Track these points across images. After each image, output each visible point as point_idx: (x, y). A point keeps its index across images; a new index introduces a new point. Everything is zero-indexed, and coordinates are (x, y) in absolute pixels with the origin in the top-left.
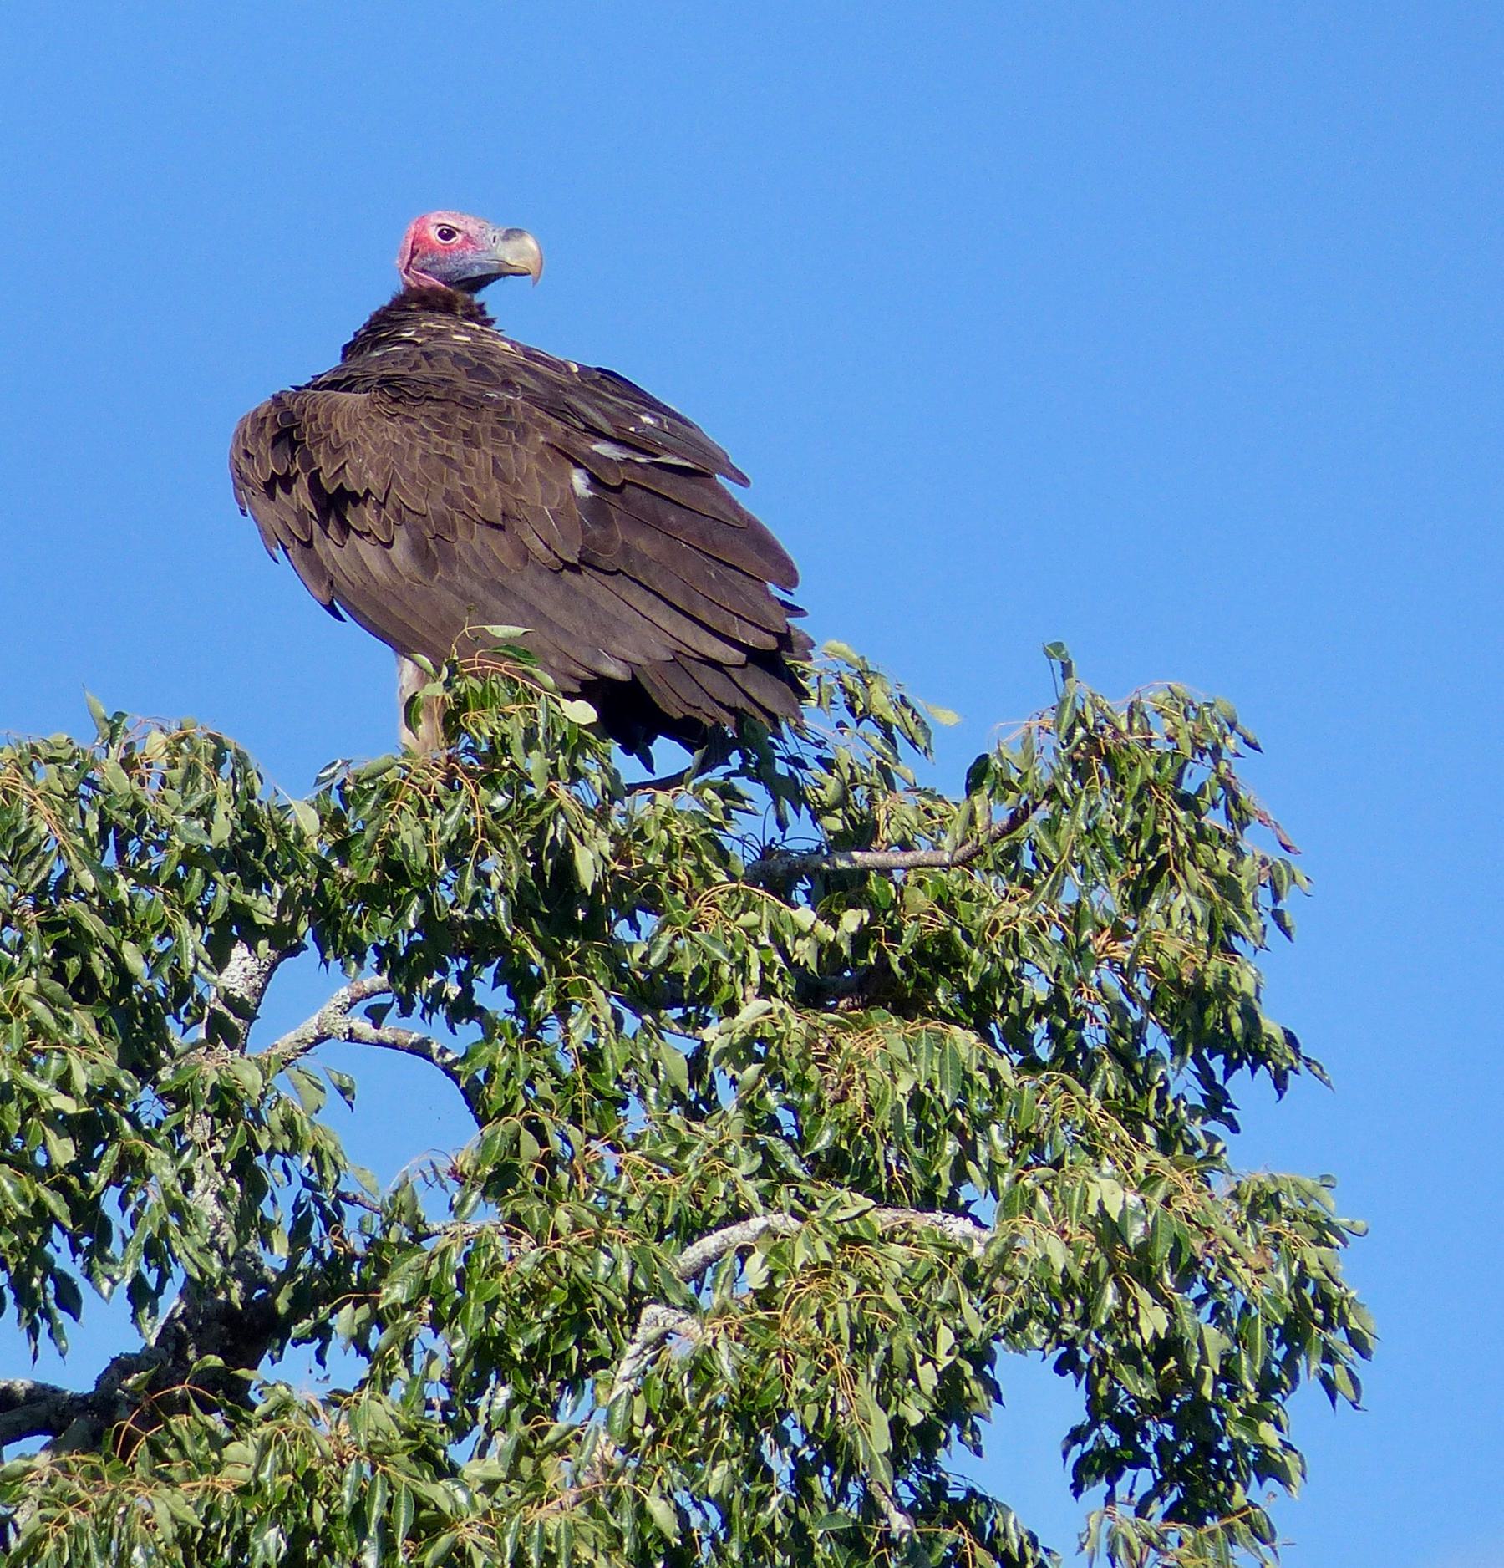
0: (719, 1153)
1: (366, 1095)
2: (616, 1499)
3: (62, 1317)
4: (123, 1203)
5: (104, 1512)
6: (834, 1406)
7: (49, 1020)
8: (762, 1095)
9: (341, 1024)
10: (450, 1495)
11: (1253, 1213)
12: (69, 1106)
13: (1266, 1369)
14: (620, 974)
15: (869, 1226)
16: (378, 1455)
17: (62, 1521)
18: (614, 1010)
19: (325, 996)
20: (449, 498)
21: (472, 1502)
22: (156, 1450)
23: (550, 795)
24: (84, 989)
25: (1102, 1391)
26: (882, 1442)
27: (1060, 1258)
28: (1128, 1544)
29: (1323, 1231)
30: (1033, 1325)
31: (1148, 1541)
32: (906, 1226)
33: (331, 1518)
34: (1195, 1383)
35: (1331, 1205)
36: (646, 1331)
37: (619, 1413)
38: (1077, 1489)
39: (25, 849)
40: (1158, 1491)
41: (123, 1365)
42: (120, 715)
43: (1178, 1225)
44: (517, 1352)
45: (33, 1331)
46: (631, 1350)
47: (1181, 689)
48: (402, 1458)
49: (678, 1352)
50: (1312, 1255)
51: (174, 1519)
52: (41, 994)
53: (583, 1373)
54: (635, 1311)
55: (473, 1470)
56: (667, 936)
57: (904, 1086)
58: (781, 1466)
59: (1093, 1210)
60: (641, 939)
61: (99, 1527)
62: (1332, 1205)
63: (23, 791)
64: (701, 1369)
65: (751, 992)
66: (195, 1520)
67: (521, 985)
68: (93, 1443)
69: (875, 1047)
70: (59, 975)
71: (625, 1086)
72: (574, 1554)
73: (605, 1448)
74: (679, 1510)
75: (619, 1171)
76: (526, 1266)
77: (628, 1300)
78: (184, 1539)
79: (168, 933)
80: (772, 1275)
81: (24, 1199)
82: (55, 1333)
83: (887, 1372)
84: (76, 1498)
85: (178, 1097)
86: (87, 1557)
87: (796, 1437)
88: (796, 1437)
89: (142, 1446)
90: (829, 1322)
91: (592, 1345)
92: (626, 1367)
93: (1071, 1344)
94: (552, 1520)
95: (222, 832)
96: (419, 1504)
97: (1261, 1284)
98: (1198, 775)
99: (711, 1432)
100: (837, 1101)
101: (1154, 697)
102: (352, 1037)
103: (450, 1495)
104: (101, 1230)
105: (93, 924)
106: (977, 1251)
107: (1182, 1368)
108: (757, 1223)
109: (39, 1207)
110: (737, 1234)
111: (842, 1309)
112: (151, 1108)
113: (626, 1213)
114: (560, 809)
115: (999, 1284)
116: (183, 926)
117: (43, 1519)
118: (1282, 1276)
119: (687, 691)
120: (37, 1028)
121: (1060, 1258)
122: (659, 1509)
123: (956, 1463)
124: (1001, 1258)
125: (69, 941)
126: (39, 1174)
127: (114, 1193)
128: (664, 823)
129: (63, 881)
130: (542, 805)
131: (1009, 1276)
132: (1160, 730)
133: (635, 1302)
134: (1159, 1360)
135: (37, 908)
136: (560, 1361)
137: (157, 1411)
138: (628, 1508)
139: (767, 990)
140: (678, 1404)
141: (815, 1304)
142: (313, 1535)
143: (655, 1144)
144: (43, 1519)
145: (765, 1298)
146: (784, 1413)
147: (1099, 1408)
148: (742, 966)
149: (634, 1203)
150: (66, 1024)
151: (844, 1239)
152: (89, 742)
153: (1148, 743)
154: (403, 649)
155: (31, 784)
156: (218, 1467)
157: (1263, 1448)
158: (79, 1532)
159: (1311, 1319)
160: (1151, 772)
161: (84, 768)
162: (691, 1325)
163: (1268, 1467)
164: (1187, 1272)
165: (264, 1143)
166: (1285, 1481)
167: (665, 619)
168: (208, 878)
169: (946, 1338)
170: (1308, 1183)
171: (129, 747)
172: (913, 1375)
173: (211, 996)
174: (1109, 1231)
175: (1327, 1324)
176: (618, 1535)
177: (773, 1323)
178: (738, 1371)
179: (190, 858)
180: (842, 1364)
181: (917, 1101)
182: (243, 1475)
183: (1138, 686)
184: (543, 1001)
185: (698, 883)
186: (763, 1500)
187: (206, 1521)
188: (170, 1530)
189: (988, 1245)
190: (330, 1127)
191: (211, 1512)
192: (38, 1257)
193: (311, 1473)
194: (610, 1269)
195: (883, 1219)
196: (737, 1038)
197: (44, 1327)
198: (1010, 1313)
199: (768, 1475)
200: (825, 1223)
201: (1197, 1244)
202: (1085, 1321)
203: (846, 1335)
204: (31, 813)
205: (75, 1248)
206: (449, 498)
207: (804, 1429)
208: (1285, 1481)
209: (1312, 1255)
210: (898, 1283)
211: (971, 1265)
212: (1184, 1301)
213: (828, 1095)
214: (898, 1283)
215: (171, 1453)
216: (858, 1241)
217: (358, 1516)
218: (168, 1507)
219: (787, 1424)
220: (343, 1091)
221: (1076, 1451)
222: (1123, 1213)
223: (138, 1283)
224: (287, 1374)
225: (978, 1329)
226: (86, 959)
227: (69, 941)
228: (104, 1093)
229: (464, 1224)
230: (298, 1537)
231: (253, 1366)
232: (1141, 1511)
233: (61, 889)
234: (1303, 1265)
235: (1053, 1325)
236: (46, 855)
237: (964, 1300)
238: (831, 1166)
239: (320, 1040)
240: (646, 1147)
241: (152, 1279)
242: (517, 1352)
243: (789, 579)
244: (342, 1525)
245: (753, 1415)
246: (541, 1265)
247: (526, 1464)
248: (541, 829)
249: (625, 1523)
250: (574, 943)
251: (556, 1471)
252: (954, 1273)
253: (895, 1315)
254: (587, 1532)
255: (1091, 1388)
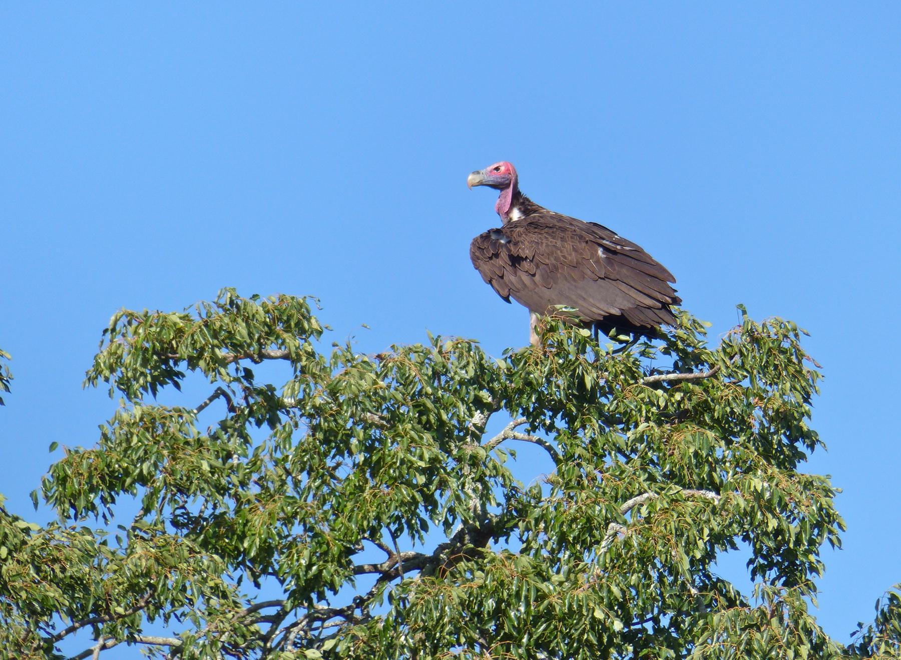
0: (634, 474)
1: (519, 455)
2: (601, 587)
3: (423, 533)
4: (441, 495)
5: (436, 595)
6: (671, 554)
7: (416, 437)
8: (646, 453)
9: (511, 434)
10: (547, 587)
11: (805, 487)
12: (422, 464)
13: (810, 537)
14: (601, 414)
15: (681, 496)
16: (524, 575)
17: (423, 599)
18: (600, 426)
19: (507, 424)
20: (556, 259)
21: (555, 589)
22: (453, 575)
23: (577, 359)
24: (427, 427)
25: (758, 546)
26: (687, 566)
27: (743, 505)
28: (768, 594)
29: (827, 492)
30: (735, 526)
31: (774, 593)
32: (693, 495)
33: (509, 595)
34: (788, 542)
35: (831, 484)
36: (610, 532)
37: (601, 559)
38: (753, 579)
39: (408, 381)
40: (778, 578)
41: (442, 548)
42: (439, 336)
43: (779, 492)
44: (571, 539)
45: (413, 537)
46: (606, 537)
47: (779, 319)
48: (532, 575)
49: (621, 538)
50: (823, 500)
51: (459, 597)
52: (413, 429)
53: (591, 546)
54: (607, 525)
55: (555, 578)
56: (615, 402)
57: (692, 450)
58: (654, 575)
59: (752, 489)
60: (607, 403)
61: (434, 600)
62: (830, 484)
63: (407, 362)
64: (627, 544)
65: (643, 419)
66: (465, 597)
67: (570, 419)
68: (432, 573)
69: (682, 437)
70: (420, 422)
71: (604, 450)
72: (588, 605)
73: (598, 570)
74: (622, 590)
75: (602, 480)
76: (572, 511)
77: (605, 521)
78: (462, 603)
79: (455, 406)
80: (650, 513)
81: (409, 495)
82: (421, 538)
83: (688, 543)
84: (427, 591)
85: (459, 460)
86: (431, 610)
87: (659, 565)
88: (659, 565)
89: (448, 573)
90: (668, 528)
91: (594, 536)
92: (603, 543)
93: (747, 532)
94: (580, 594)
95: (471, 373)
96: (538, 590)
97: (807, 510)
98: (786, 345)
99: (631, 564)
100: (670, 455)
101: (770, 321)
102: (515, 438)
103: (547, 587)
104: (435, 504)
105: (430, 405)
106: (716, 503)
107: (783, 539)
108: (645, 495)
109: (413, 498)
110: (639, 499)
111: (672, 523)
112: (451, 464)
113: (604, 493)
114: (580, 363)
115: (723, 513)
116: (460, 404)
117: (417, 598)
118: (814, 508)
119: (642, 317)
120: (413, 440)
121: (743, 505)
122: (615, 590)
123: (713, 569)
124: (724, 504)
125: (423, 411)
126: (414, 487)
127: (438, 492)
128: (614, 366)
129: (420, 391)
130: (574, 362)
131: (726, 510)
132: (773, 332)
133: (607, 522)
134: (776, 536)
135: (412, 400)
136: (584, 542)
137: (452, 563)
138: (605, 590)
139: (647, 419)
140: (620, 555)
141: (663, 522)
142: (504, 601)
143: (613, 471)
144: (417, 598)
145: (648, 520)
146: (654, 558)
147: (757, 552)
148: (640, 411)
149: (607, 490)
150: (421, 438)
151: (672, 500)
152: (428, 345)
153: (769, 337)
154: (532, 310)
155: (410, 360)
156: (473, 580)
157: (810, 563)
158: (428, 601)
159: (825, 521)
160: (771, 345)
161: (426, 354)
162: (624, 529)
163: (813, 569)
164: (784, 508)
165: (488, 473)
166: (818, 573)
167: (633, 293)
168: (467, 388)
169: (706, 531)
170: (822, 478)
171: (441, 347)
172: (696, 543)
173: (470, 425)
174: (758, 496)
175: (829, 522)
176: (602, 598)
177: (650, 529)
178: (639, 545)
179: (461, 383)
180: (673, 541)
181: (696, 454)
182: (480, 582)
183: (763, 318)
184: (577, 424)
185: (625, 385)
186: (648, 586)
187: (469, 598)
188: (457, 600)
189: (720, 500)
190: (509, 467)
191: (471, 595)
192: (414, 514)
193: (502, 581)
194: (600, 511)
195: (686, 493)
196: (638, 435)
197: (417, 536)
198: (727, 522)
199: (650, 578)
200: (665, 495)
201: (787, 498)
202: (751, 524)
203: (674, 532)
204: (410, 369)
205: (426, 510)
206: (556, 259)
207: (661, 562)
208: (818, 573)
209: (823, 500)
210: (690, 514)
211: (714, 507)
212: (783, 516)
213: (668, 453)
214: (690, 514)
215: (458, 576)
216: (677, 501)
217: (518, 595)
218: (457, 592)
219: (656, 561)
220: (512, 455)
221: (751, 567)
222: (762, 490)
223: (446, 520)
224: (494, 548)
225: (717, 529)
226: (428, 416)
227: (423, 411)
228: (434, 460)
229: (551, 497)
230: (499, 602)
231: (484, 546)
232: (773, 583)
233: (420, 393)
234: (821, 504)
235: (741, 525)
236: (415, 383)
237: (712, 519)
238: (671, 476)
239: (504, 439)
240: (610, 472)
241: (450, 519)
242: (571, 539)
243: (674, 281)
244: (513, 597)
245: (645, 559)
246: (577, 511)
247: (572, 576)
248: (575, 370)
249: (604, 594)
250: (586, 405)
251: (582, 578)
252: (708, 510)
253: (689, 525)
254: (592, 598)
255: (754, 546)
